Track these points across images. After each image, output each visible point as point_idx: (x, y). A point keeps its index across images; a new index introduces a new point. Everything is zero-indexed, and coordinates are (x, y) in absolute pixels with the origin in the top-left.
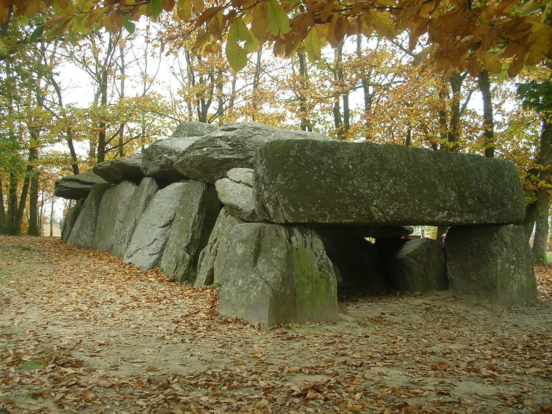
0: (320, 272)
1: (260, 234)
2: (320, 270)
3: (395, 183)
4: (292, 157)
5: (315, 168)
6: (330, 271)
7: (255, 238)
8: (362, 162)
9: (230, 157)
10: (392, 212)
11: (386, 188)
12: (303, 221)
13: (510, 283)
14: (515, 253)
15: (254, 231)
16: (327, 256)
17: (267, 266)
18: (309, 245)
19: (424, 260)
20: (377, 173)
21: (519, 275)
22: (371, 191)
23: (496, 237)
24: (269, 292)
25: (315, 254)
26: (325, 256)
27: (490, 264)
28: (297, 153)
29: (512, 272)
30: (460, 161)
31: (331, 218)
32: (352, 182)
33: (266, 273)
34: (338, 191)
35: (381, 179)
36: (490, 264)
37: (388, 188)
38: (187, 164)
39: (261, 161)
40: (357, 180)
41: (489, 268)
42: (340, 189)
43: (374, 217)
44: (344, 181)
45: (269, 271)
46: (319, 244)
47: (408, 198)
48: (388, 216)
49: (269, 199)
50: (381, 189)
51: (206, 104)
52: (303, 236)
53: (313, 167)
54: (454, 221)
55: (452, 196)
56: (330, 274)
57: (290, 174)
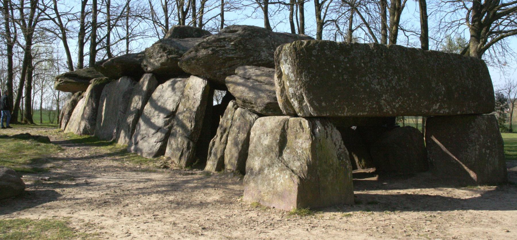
0: (339, 160)
1: (284, 126)
2: (339, 158)
4: (314, 56)
5: (334, 66)
7: (279, 130)
9: (233, 56)
11: (392, 84)
12: (325, 115)
15: (278, 123)
16: (344, 146)
17: (292, 156)
18: (329, 136)
20: (385, 71)
24: (296, 180)
26: (343, 146)
28: (318, 53)
31: (348, 112)
33: (292, 162)
37: (394, 83)
38: (193, 62)
39: (286, 61)
40: (369, 77)
42: (356, 85)
44: (358, 77)
45: (295, 160)
46: (337, 135)
48: (394, 108)
49: (294, 95)
51: (185, 10)
52: (325, 129)
53: (333, 66)
54: (444, 112)
55: (443, 90)
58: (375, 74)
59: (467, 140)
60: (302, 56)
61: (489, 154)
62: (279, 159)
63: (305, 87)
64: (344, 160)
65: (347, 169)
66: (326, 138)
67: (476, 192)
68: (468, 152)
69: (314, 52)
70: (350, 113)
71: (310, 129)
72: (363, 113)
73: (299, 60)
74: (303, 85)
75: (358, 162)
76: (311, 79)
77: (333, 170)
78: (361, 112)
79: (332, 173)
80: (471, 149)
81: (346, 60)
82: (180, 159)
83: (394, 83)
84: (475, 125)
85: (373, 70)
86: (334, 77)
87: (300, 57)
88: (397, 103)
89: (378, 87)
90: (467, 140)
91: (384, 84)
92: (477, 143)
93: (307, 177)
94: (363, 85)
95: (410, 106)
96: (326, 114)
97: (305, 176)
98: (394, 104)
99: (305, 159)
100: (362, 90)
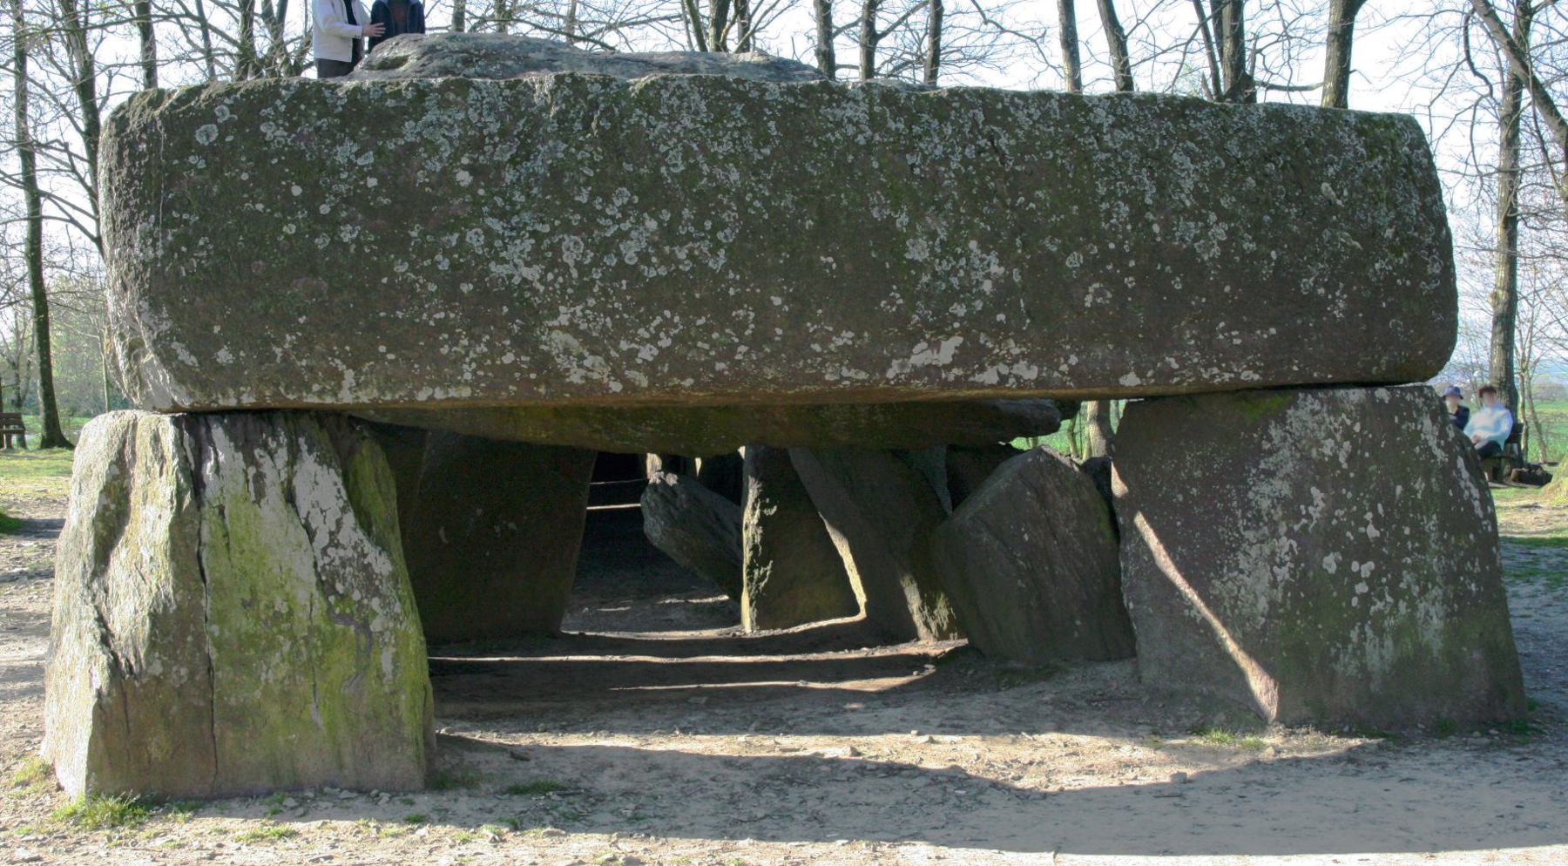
0: (326, 595)
1: (121, 453)
2: (326, 586)
3: (669, 233)
4: (201, 151)
6: (371, 589)
8: (525, 153)
10: (647, 353)
13: (1349, 640)
14: (1374, 509)
19: (1026, 537)
20: (584, 199)
21: (1402, 605)
22: (546, 271)
23: (1276, 441)
25: (307, 527)
27: (1246, 553)
29: (1361, 588)
30: (1058, 124)
32: (462, 239)
34: (394, 275)
35: (602, 222)
36: (1246, 553)
37: (631, 258)
41: (1242, 572)
42: (401, 268)
43: (561, 375)
44: (423, 234)
47: (732, 292)
50: (596, 263)
52: (250, 460)
53: (289, 186)
56: (375, 603)
57: (185, 216)
58: (526, 216)
59: (1239, 513)
60: (142, 155)
61: (1368, 581)
62: (89, 587)
63: (142, 285)
64: (356, 596)
65: (369, 634)
66: (258, 502)
67: (1195, 755)
68: (1242, 572)
69: (205, 135)
70: (376, 394)
71: (177, 460)
72: (445, 388)
73: (129, 173)
74: (132, 274)
75: (921, 610)
76: (171, 249)
77: (294, 639)
78: (433, 384)
79: (286, 648)
80: (1254, 552)
81: (367, 160)
82: (395, 587)
83: (631, 253)
84: (1284, 439)
85: (523, 199)
86: (288, 237)
87: (135, 157)
88: (643, 342)
89: (532, 273)
90: (1239, 513)
91: (568, 258)
92: (1283, 529)
93: (149, 664)
94: (444, 265)
95: (734, 352)
96: (238, 396)
97: (138, 660)
98: (624, 345)
99: (155, 590)
100: (432, 288)
